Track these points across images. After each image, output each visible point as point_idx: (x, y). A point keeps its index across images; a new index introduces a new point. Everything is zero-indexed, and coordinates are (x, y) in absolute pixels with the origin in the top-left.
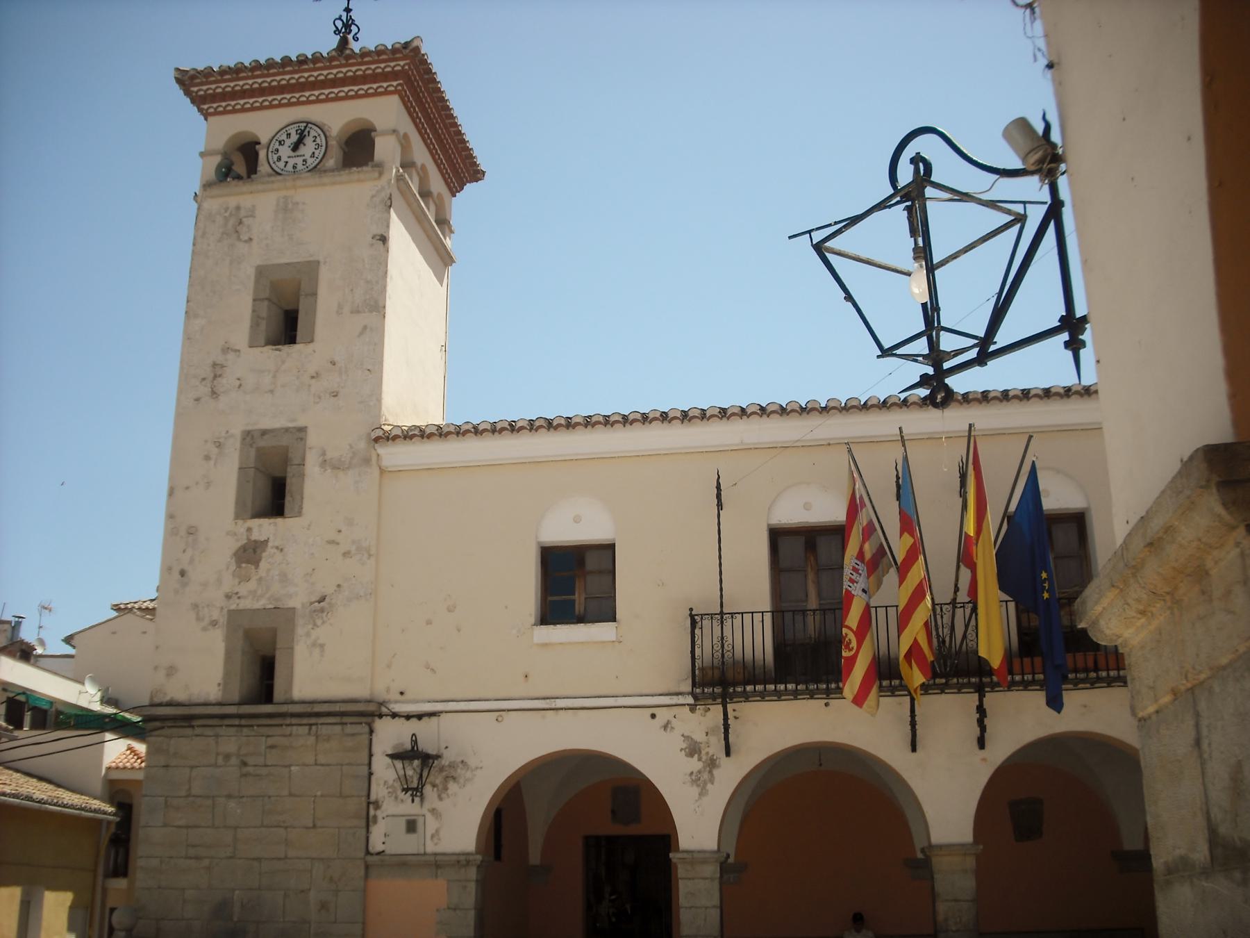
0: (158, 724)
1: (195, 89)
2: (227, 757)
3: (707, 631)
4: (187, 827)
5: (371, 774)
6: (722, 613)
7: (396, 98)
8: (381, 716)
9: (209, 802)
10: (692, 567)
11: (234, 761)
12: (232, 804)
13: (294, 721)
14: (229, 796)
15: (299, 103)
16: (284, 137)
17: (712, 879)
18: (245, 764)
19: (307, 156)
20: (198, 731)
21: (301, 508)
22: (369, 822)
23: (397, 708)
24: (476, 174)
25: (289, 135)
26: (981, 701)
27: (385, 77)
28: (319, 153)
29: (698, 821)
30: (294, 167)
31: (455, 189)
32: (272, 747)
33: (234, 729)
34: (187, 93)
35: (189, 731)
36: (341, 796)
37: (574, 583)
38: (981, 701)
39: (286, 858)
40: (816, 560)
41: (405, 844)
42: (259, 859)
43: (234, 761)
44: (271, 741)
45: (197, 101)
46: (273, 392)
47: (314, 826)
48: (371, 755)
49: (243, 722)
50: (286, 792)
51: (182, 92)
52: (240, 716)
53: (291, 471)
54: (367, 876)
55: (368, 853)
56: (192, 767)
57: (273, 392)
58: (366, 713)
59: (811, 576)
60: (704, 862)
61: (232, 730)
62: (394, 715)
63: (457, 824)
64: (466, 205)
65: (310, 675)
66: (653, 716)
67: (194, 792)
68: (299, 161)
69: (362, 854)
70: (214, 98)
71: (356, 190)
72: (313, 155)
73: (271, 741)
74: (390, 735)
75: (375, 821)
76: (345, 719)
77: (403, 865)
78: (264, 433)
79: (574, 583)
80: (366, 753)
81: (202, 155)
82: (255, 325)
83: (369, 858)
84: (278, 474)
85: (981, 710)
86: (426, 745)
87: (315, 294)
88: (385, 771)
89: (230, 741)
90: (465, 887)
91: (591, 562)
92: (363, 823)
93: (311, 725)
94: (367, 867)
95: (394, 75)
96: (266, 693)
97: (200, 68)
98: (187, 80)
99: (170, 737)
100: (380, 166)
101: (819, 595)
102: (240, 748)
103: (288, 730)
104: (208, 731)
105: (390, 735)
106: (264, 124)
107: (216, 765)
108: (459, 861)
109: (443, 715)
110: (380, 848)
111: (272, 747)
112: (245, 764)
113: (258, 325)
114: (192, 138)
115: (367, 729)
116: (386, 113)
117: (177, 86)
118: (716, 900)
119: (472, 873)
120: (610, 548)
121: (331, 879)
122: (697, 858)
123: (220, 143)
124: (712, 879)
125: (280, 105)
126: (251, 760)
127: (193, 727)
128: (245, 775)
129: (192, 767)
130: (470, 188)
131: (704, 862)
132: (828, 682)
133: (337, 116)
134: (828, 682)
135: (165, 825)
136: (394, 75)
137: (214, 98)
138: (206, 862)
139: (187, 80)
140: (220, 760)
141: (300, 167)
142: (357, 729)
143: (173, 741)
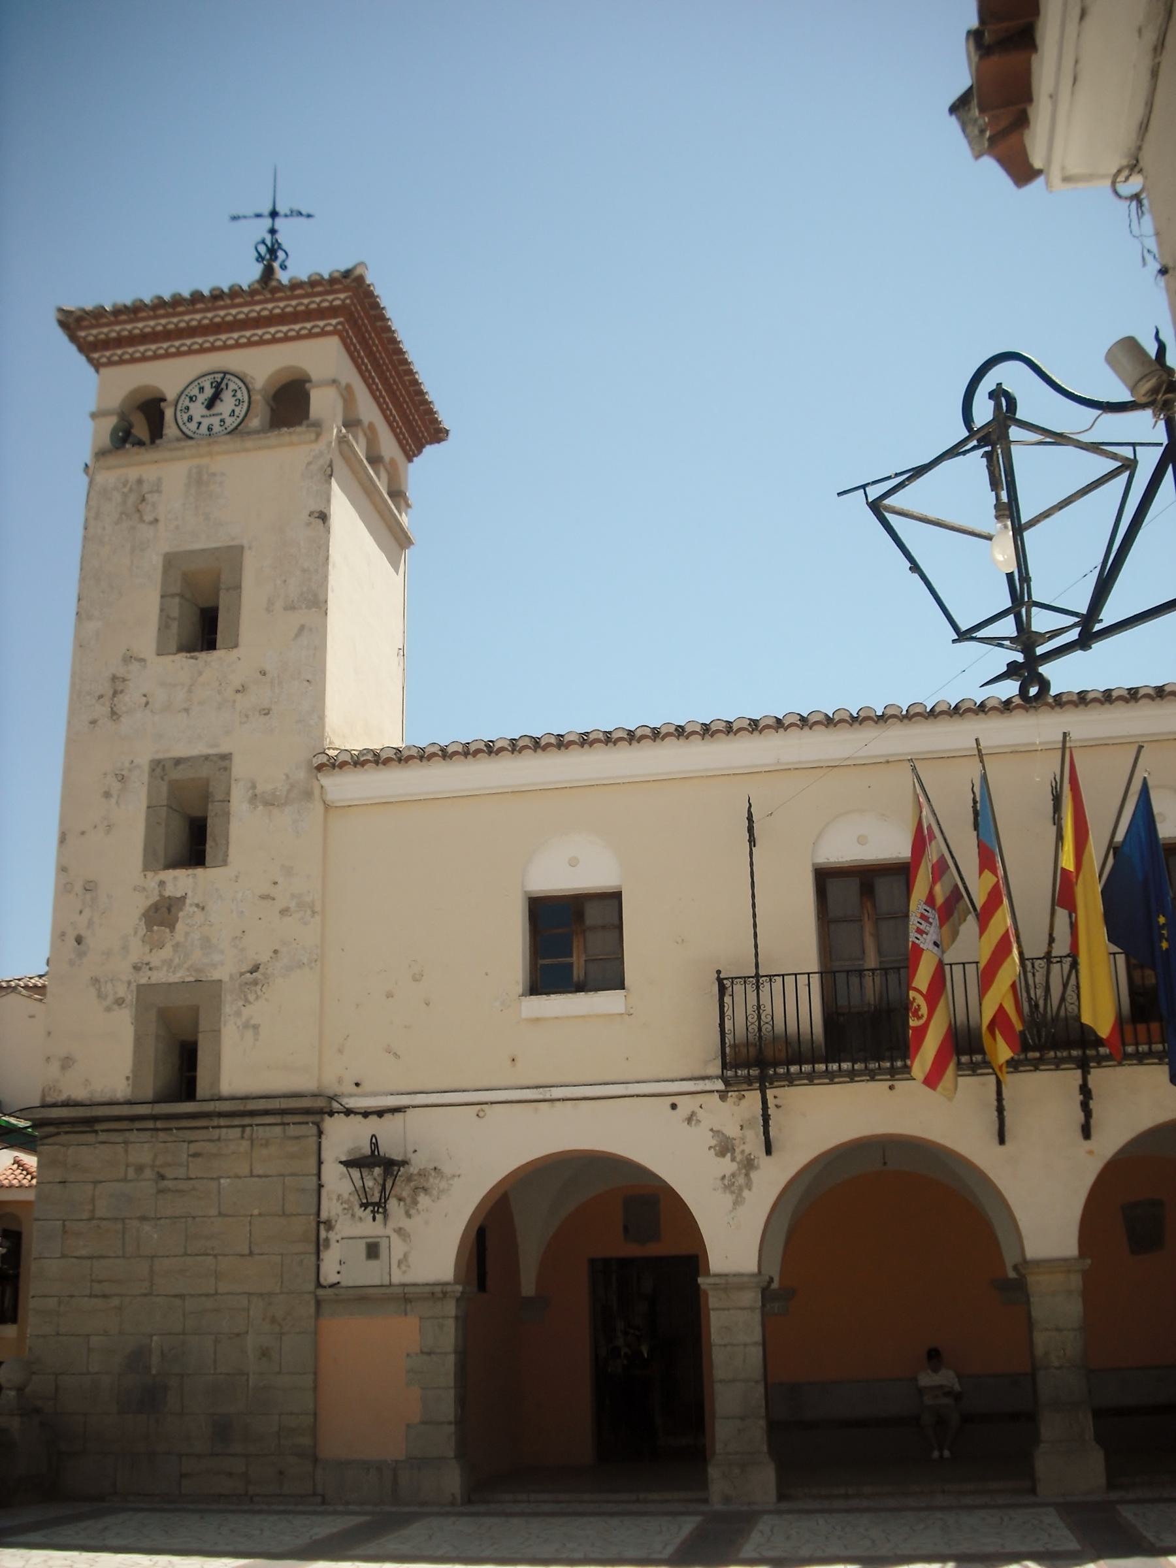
0: (51, 1129)
2: (140, 1169)
3: (740, 998)
4: (91, 1258)
6: (757, 976)
8: (331, 1114)
9: (119, 1226)
11: (148, 1173)
12: (147, 1227)
13: (223, 1122)
14: (143, 1219)
15: (213, 349)
16: (195, 391)
17: (752, 1309)
18: (162, 1177)
19: (226, 416)
20: (103, 1137)
21: (226, 855)
22: (319, 1246)
23: (352, 1103)
25: (202, 389)
27: (321, 313)
28: (241, 411)
29: (733, 1237)
30: (210, 429)
32: (196, 1155)
33: (149, 1133)
34: (73, 338)
35: (90, 1138)
36: (284, 1214)
37: (570, 941)
39: (216, 1293)
40: (874, 906)
41: (367, 1274)
42: (181, 1296)
43: (148, 1173)
44: (194, 1148)
45: (85, 348)
46: (188, 710)
47: (251, 1254)
49: (159, 1125)
50: (213, 1212)
52: (155, 1118)
53: (213, 809)
55: (319, 1285)
56: (96, 1183)
57: (188, 710)
58: (312, 1111)
59: (868, 927)
60: (741, 1287)
63: (430, 1245)
65: (241, 1064)
66: (674, 1106)
67: (98, 1214)
68: (215, 421)
69: (311, 1287)
70: (106, 344)
73: (194, 1148)
74: (344, 1138)
77: (364, 1299)
78: (178, 762)
79: (570, 941)
80: (313, 1161)
81: (93, 416)
82: (164, 627)
83: (320, 1292)
84: (197, 813)
85: (1085, 1091)
86: (388, 1149)
89: (143, 1150)
90: (441, 1327)
91: (592, 915)
92: (312, 1248)
93: (244, 1126)
94: (318, 1303)
95: (332, 312)
101: (880, 952)
102: (156, 1156)
103: (215, 1133)
105: (344, 1138)
106: (170, 376)
107: (125, 1180)
108: (434, 1293)
111: (196, 1155)
113: (167, 627)
115: (314, 1130)
116: (323, 358)
118: (757, 1335)
119: (451, 1308)
121: (273, 1320)
122: (731, 1283)
123: (115, 400)
124: (752, 1309)
125: (190, 352)
126: (169, 1175)
127: (96, 1132)
128: (160, 1191)
129: (96, 1183)
131: (741, 1287)
133: (262, 364)
135: (63, 1256)
136: (332, 312)
137: (106, 344)
138: (115, 1302)
139: (73, 324)
140: (131, 1173)
143: (72, 1150)
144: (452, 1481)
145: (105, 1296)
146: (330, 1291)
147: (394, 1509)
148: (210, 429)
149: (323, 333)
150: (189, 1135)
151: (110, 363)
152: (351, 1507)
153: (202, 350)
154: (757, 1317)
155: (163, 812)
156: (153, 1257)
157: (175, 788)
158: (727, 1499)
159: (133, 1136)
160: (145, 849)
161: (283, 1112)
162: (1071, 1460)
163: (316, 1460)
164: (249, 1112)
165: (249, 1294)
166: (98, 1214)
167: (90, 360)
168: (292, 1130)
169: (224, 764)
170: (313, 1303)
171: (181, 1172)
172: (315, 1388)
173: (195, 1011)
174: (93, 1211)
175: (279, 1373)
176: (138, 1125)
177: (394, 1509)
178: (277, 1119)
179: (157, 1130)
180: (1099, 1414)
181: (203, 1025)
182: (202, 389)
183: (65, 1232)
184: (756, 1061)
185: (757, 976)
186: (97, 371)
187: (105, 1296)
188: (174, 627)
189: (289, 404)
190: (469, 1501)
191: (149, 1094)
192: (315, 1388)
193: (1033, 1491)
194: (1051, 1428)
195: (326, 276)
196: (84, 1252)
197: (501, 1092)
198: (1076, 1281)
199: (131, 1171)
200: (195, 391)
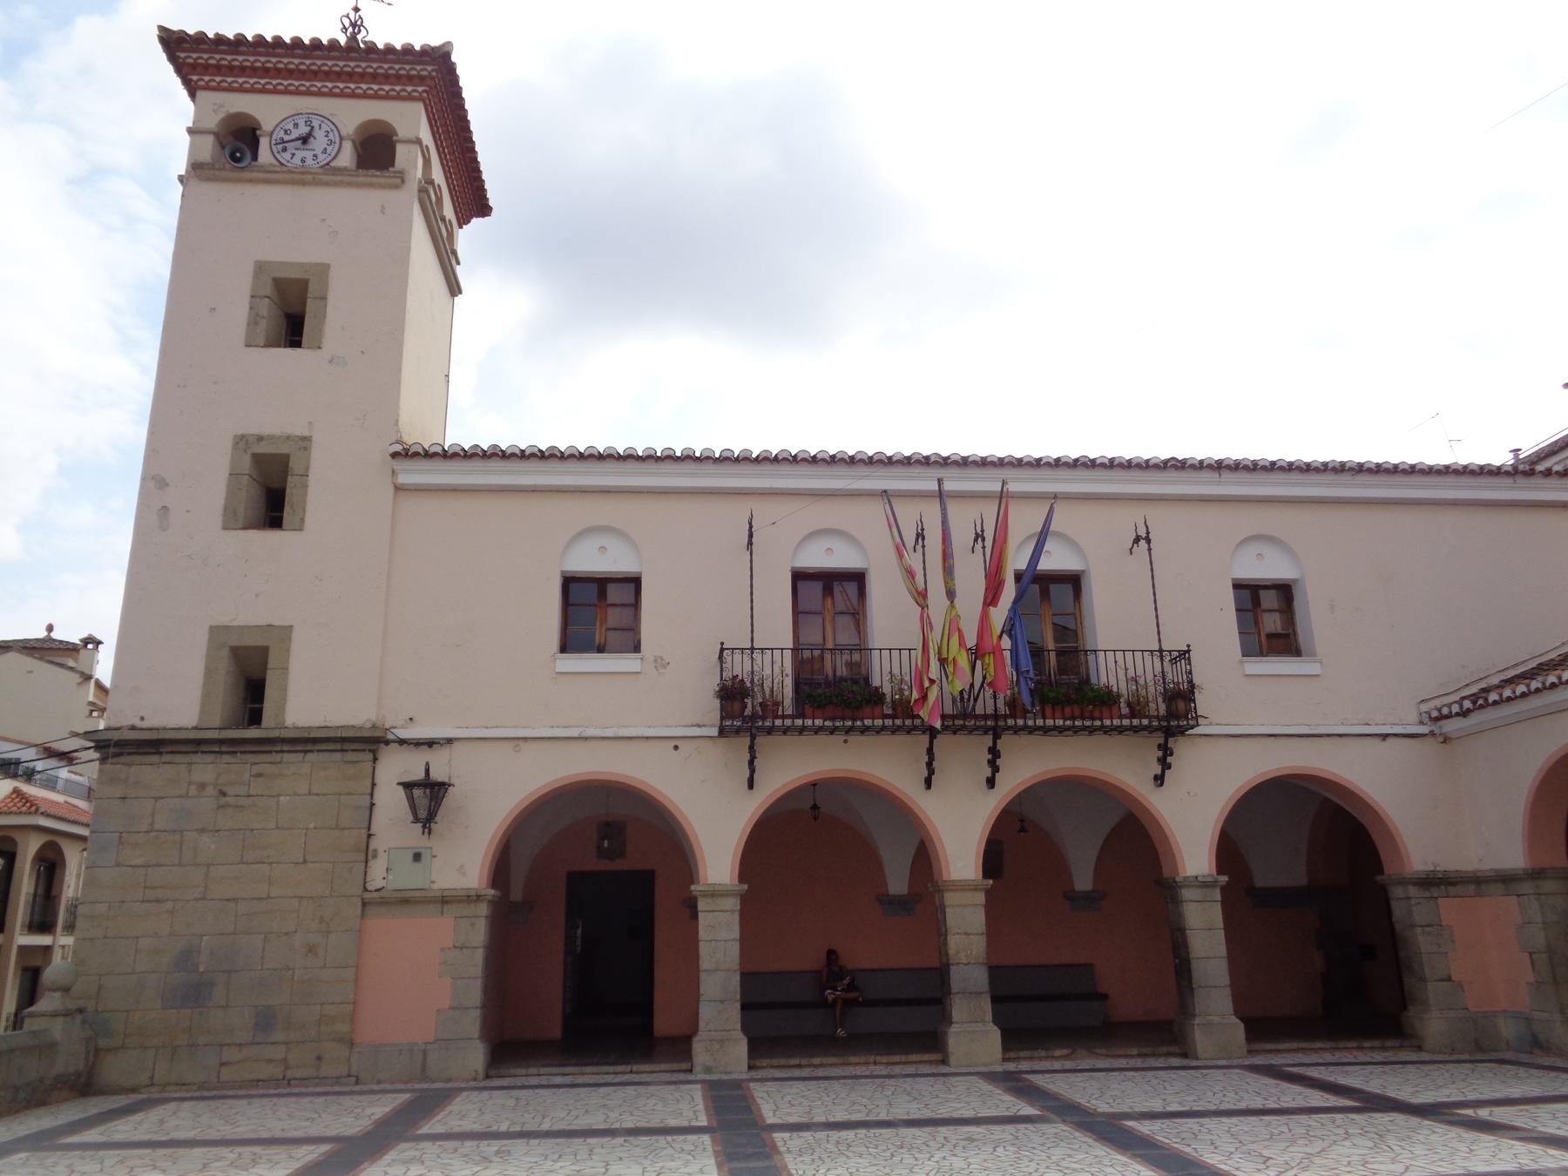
1: (183, 55)
2: (202, 786)
4: (146, 866)
5: (373, 805)
6: (752, 649)
7: (420, 107)
8: (387, 742)
9: (177, 837)
10: (715, 608)
11: (210, 791)
12: (205, 838)
14: (202, 831)
15: (308, 93)
16: (290, 126)
17: (732, 911)
18: (224, 794)
19: (318, 151)
20: (167, 758)
21: (303, 520)
23: (403, 734)
24: (483, 209)
25: (296, 125)
26: (931, 743)
27: (410, 79)
28: (332, 150)
31: (463, 220)
32: (259, 775)
34: (172, 58)
35: (155, 759)
36: (337, 827)
37: (597, 611)
38: (931, 743)
39: (269, 897)
41: (406, 878)
42: (235, 900)
43: (210, 791)
44: (256, 769)
45: (182, 69)
46: (279, 394)
47: (305, 861)
48: (374, 785)
50: (272, 825)
51: (164, 56)
52: (221, 742)
53: (292, 482)
54: (363, 916)
55: (365, 889)
56: (157, 799)
57: (279, 394)
58: (370, 743)
61: (211, 758)
62: (402, 742)
63: (464, 859)
64: (470, 237)
65: (302, 702)
66: (676, 748)
67: (157, 827)
68: (309, 155)
69: (359, 892)
70: (206, 68)
71: (359, 205)
72: (325, 151)
73: (256, 769)
74: (395, 768)
75: (375, 857)
76: (347, 746)
77: (405, 901)
78: (260, 439)
79: (597, 611)
80: (368, 783)
81: (190, 131)
82: (253, 321)
83: (367, 895)
84: (276, 485)
85: (930, 752)
86: (437, 775)
87: (324, 298)
88: (391, 802)
89: (205, 770)
90: (473, 925)
92: (362, 857)
94: (364, 904)
95: (421, 80)
96: (255, 718)
97: (191, 32)
98: (175, 44)
99: (130, 765)
100: (401, 177)
102: (219, 775)
103: (277, 757)
104: (178, 758)
105: (410, 765)
106: (270, 110)
107: (187, 796)
108: (471, 898)
109: (456, 745)
110: (379, 883)
111: (259, 775)
112: (224, 794)
113: (256, 323)
114: (169, 116)
115: (371, 756)
116: (411, 121)
117: (159, 47)
119: (483, 909)
120: (635, 582)
121: (322, 920)
123: (212, 122)
124: (732, 911)
125: (286, 92)
126: (230, 790)
128: (221, 807)
129: (157, 799)
130: (476, 222)
132: (854, 720)
133: (352, 114)
134: (854, 720)
135: (118, 865)
136: (421, 80)
137: (206, 68)
138: (169, 905)
139: (175, 44)
140: (193, 790)
141: (309, 162)
142: (360, 756)
143: (133, 769)
144: (477, 1056)
145: (158, 901)
146: (376, 895)
147: (425, 1086)
148: (303, 161)
149: (410, 98)
150: (252, 758)
151: (207, 88)
152: (383, 1086)
153: (297, 93)
154: (736, 916)
155: (245, 479)
156: (208, 865)
157: (258, 459)
158: (708, 1070)
159: (197, 758)
160: (226, 509)
161: (343, 740)
162: (974, 1032)
163: (352, 1044)
164: (307, 742)
165: (301, 898)
166: (157, 827)
167: (187, 83)
168: (350, 756)
169: (304, 444)
170: (359, 904)
171: (243, 790)
172: (356, 981)
173: (264, 651)
174: (152, 824)
175: (324, 967)
176: (318, 747)
177: (425, 1086)
178: (338, 746)
179: (221, 753)
180: (995, 1000)
181: (272, 662)
182: (296, 125)
183: (121, 842)
184: (741, 710)
185: (1161, 651)
186: (192, 95)
187: (158, 901)
188: (263, 324)
189: (376, 151)
190: (487, 1077)
191: (216, 721)
192: (356, 981)
193: (944, 1062)
194: (959, 1009)
195: (417, 48)
196: (139, 861)
197: (527, 726)
198: (981, 898)
199: (193, 787)
200: (290, 126)
